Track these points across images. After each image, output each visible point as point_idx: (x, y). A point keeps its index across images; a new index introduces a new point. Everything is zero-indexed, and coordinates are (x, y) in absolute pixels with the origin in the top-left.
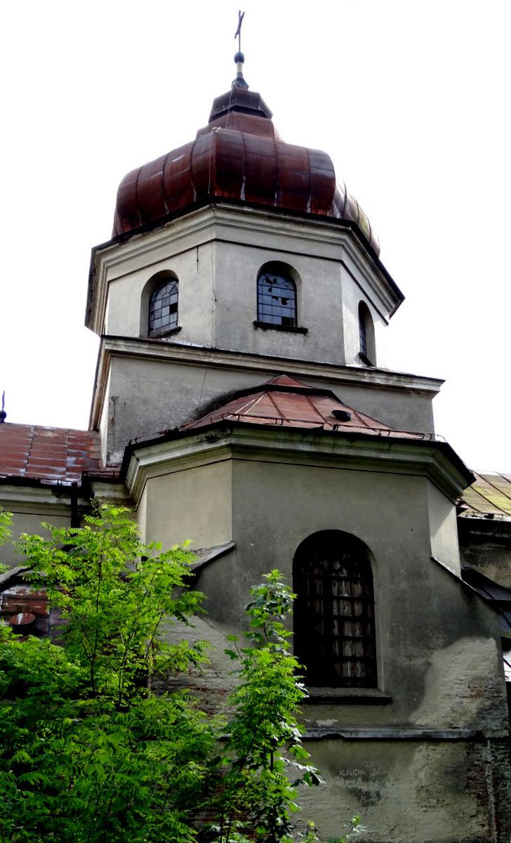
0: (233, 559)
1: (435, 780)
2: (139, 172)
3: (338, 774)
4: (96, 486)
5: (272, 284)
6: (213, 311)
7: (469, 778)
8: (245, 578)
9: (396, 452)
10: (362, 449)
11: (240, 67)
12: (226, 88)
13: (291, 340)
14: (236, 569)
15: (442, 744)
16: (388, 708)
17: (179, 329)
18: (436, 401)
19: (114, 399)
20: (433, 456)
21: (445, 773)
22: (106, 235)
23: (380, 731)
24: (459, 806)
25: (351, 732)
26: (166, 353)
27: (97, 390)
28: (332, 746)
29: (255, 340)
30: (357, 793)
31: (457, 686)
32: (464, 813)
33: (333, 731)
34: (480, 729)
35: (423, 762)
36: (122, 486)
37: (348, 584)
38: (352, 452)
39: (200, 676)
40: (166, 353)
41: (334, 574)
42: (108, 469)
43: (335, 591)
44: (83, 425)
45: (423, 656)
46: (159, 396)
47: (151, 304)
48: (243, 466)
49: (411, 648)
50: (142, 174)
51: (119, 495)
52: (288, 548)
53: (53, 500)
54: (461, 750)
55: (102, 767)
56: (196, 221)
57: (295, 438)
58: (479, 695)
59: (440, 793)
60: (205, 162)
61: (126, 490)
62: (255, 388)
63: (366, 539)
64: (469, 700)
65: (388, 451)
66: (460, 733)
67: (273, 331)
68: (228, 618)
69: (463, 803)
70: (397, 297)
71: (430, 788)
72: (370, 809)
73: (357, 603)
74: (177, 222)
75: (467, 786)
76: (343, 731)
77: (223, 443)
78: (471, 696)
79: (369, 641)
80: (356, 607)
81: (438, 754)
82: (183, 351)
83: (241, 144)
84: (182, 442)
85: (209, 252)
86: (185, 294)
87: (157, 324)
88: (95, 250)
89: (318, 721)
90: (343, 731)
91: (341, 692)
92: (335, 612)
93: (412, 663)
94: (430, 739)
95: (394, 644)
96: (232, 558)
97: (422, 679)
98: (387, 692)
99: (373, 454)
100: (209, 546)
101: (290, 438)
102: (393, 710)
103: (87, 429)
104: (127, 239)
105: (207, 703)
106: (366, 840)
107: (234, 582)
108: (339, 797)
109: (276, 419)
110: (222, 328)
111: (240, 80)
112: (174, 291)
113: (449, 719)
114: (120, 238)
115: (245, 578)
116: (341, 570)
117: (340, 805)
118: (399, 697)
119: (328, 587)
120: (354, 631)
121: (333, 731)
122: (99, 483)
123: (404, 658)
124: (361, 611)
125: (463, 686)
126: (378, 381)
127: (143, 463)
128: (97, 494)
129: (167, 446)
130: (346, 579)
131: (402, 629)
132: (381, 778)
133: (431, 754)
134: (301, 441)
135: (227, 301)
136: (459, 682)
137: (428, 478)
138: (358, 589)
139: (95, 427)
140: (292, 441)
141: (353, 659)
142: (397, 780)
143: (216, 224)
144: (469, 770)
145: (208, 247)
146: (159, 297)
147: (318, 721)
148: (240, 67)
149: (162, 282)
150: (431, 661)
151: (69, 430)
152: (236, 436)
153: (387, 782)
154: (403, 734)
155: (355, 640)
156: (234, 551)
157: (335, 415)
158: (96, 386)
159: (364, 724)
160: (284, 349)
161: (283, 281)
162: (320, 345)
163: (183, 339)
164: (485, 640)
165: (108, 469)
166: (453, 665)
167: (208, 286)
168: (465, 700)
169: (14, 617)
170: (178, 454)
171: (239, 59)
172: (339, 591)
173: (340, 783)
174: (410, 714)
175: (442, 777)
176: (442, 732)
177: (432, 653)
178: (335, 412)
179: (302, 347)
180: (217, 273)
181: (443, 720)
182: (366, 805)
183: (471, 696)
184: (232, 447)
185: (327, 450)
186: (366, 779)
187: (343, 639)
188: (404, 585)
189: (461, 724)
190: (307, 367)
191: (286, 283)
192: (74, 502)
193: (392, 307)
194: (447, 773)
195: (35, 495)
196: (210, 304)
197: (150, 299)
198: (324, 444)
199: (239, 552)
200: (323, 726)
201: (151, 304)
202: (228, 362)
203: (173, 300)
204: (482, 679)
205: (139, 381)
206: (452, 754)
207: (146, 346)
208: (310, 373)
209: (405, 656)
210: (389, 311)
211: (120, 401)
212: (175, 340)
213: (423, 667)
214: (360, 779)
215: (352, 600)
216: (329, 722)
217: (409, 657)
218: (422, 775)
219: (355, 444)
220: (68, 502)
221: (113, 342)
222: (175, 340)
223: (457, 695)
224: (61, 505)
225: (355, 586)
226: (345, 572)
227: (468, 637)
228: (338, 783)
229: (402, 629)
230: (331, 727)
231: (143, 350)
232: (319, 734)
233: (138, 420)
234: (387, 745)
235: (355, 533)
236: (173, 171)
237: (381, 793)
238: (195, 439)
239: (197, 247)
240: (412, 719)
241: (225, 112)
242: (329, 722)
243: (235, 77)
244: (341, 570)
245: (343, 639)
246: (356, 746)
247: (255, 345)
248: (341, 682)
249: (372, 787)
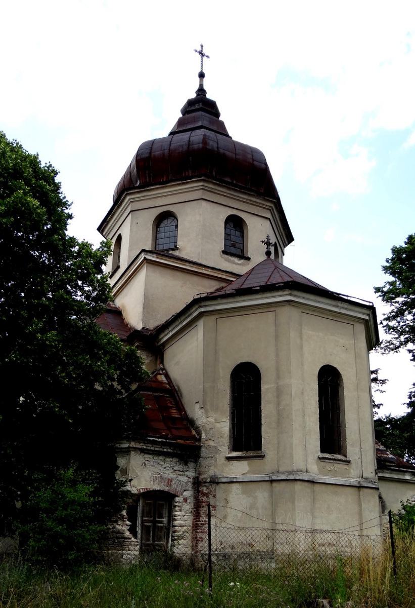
2: (153, 142)
12: (193, 95)
50: (155, 146)
62: (182, 310)
111: (201, 91)
143: (203, 189)
149: (165, 218)
171: (202, 75)
212: (176, 253)
243: (197, 87)
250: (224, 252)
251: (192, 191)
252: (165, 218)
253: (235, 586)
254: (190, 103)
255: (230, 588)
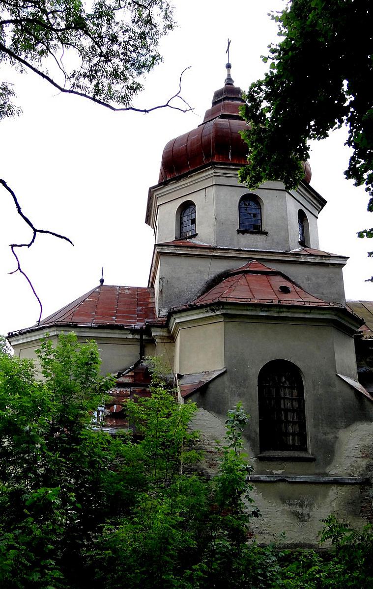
0: (225, 378)
1: (341, 507)
2: (174, 142)
3: (285, 502)
4: (152, 330)
5: (247, 206)
6: (214, 225)
7: (362, 507)
8: (232, 388)
9: (313, 313)
10: (294, 312)
11: (229, 71)
12: (221, 85)
13: (259, 239)
14: (227, 383)
15: (345, 486)
16: (313, 464)
17: (197, 234)
18: (343, 269)
19: (161, 279)
20: (336, 315)
21: (347, 504)
22: (156, 183)
23: (309, 478)
24: (356, 524)
25: (292, 478)
26: (190, 251)
27: (153, 268)
28: (282, 486)
29: (238, 240)
30: (296, 514)
31: (353, 451)
32: (359, 528)
33: (282, 477)
34: (368, 477)
35: (335, 496)
36: (167, 329)
37: (289, 390)
38: (289, 315)
39: (209, 444)
40: (190, 251)
41: (281, 385)
42: (159, 319)
43: (282, 393)
44: (144, 284)
45: (333, 433)
46: (186, 276)
47: (181, 218)
48: (230, 325)
49: (326, 428)
51: (165, 334)
52: (254, 371)
53: (131, 336)
54: (357, 490)
55: (132, 82)
56: (204, 174)
57: (258, 309)
58: (367, 457)
59: (344, 515)
60: (209, 139)
61: (169, 332)
63: (299, 364)
64: (361, 459)
65: (309, 313)
66: (356, 479)
67: (248, 234)
68: (223, 411)
69: (359, 522)
70: (322, 202)
71: (339, 512)
72: (304, 523)
73: (295, 401)
74: (194, 175)
75: (361, 512)
76: (288, 477)
77: (219, 313)
78: (362, 457)
79: (303, 426)
80: (295, 403)
81: (343, 491)
82: (199, 250)
83: (228, 128)
84: (198, 311)
85: (212, 191)
86: (199, 215)
87: (185, 230)
88: (150, 189)
89: (273, 471)
90: (288, 477)
91: (286, 454)
92: (282, 406)
93: (327, 437)
94: (338, 483)
95: (316, 426)
96: (225, 377)
97: (333, 446)
98: (313, 454)
99: (301, 316)
100: (212, 370)
101: (255, 309)
102: (316, 465)
103: (146, 286)
104: (168, 183)
105: (213, 460)
106: (302, 542)
107: (226, 391)
108: (286, 516)
109: (247, 299)
110: (219, 235)
111: (229, 82)
112: (194, 211)
113: (349, 471)
114: (163, 183)
115: (232, 388)
116: (285, 382)
117: (287, 521)
118: (320, 457)
119: (278, 393)
120: (293, 418)
121: (282, 477)
122: (155, 328)
123: (322, 434)
124: (297, 406)
125: (357, 451)
126: (309, 260)
127: (177, 321)
128: (153, 334)
129: (190, 313)
130: (288, 388)
131: (320, 417)
132: (310, 505)
133: (339, 492)
134: (261, 310)
135: (222, 219)
136: (355, 448)
137: (334, 327)
138: (295, 392)
139: (152, 286)
140: (256, 310)
141: (293, 434)
142: (319, 507)
144: (362, 502)
145: (211, 188)
146: (185, 214)
147: (273, 471)
148: (229, 71)
149: (187, 207)
150: (337, 436)
151: (138, 288)
152: (225, 309)
153: (313, 508)
154: (322, 480)
155: (294, 423)
156: (226, 374)
157: (281, 289)
158: (152, 267)
159: (300, 473)
160: (255, 244)
161: (254, 203)
162: (275, 240)
163: (199, 240)
164: (370, 423)
165: (159, 319)
166: (351, 438)
167: (211, 214)
168: (359, 459)
169: (112, 408)
170: (195, 317)
171: (229, 66)
172: (285, 394)
173: (287, 508)
174: (326, 467)
175: (346, 506)
176: (345, 479)
177: (338, 431)
178: (281, 288)
179: (265, 242)
180: (216, 203)
181: (346, 471)
182: (302, 521)
183: (362, 457)
184: (224, 315)
185: (275, 314)
186: (301, 505)
187: (287, 422)
188: (321, 391)
189: (356, 474)
190: (267, 254)
191: (255, 205)
192: (141, 337)
193: (320, 208)
194: (348, 503)
195: (121, 334)
196: (213, 221)
197: (181, 216)
198: (274, 311)
199: (228, 373)
200: (276, 474)
201: (181, 218)
202: (223, 255)
203: (193, 217)
204: (368, 447)
205: (175, 268)
206: (351, 492)
207: (179, 249)
208: (270, 258)
209: (322, 433)
210: (318, 210)
211: (165, 280)
212: (194, 241)
213: (333, 439)
214: (298, 506)
215: (292, 400)
216: (280, 472)
217: (325, 434)
218: (334, 504)
219: (290, 310)
220: (138, 337)
221: (161, 247)
222: (194, 241)
223: (354, 456)
224: (134, 339)
225: (294, 391)
226: (287, 383)
227: (359, 421)
228: (285, 507)
229: (320, 417)
230: (281, 474)
231: (177, 251)
232: (274, 479)
233: (175, 290)
234: (313, 486)
235: (292, 361)
236: (192, 144)
237: (310, 514)
238: (205, 310)
239: (206, 188)
240: (327, 470)
241: (220, 101)
242: (280, 472)
243: (226, 77)
244: (285, 382)
245: (287, 422)
246: (296, 486)
247: (238, 243)
248: (287, 448)
249: (305, 511)
250: (239, 231)
251: (206, 179)
252: (187, 207)
253: (362, 560)
254: (218, 94)
255: (282, 575)
